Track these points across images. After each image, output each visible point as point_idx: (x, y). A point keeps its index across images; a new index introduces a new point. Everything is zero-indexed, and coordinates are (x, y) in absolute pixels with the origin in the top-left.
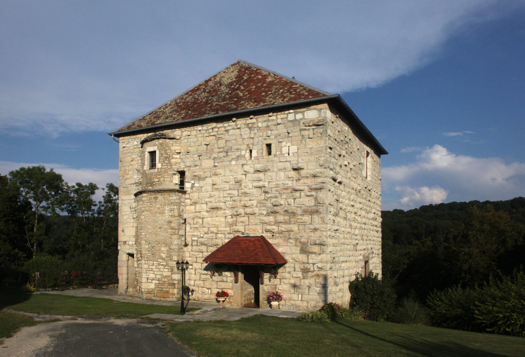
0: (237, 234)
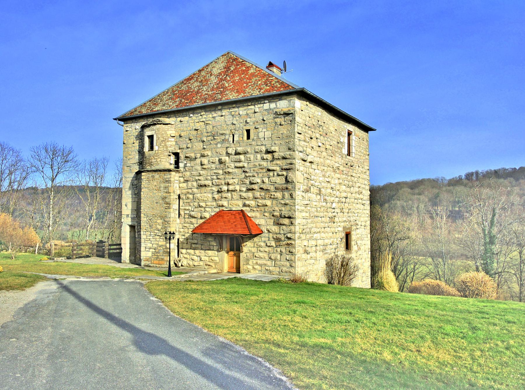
0: (221, 208)
